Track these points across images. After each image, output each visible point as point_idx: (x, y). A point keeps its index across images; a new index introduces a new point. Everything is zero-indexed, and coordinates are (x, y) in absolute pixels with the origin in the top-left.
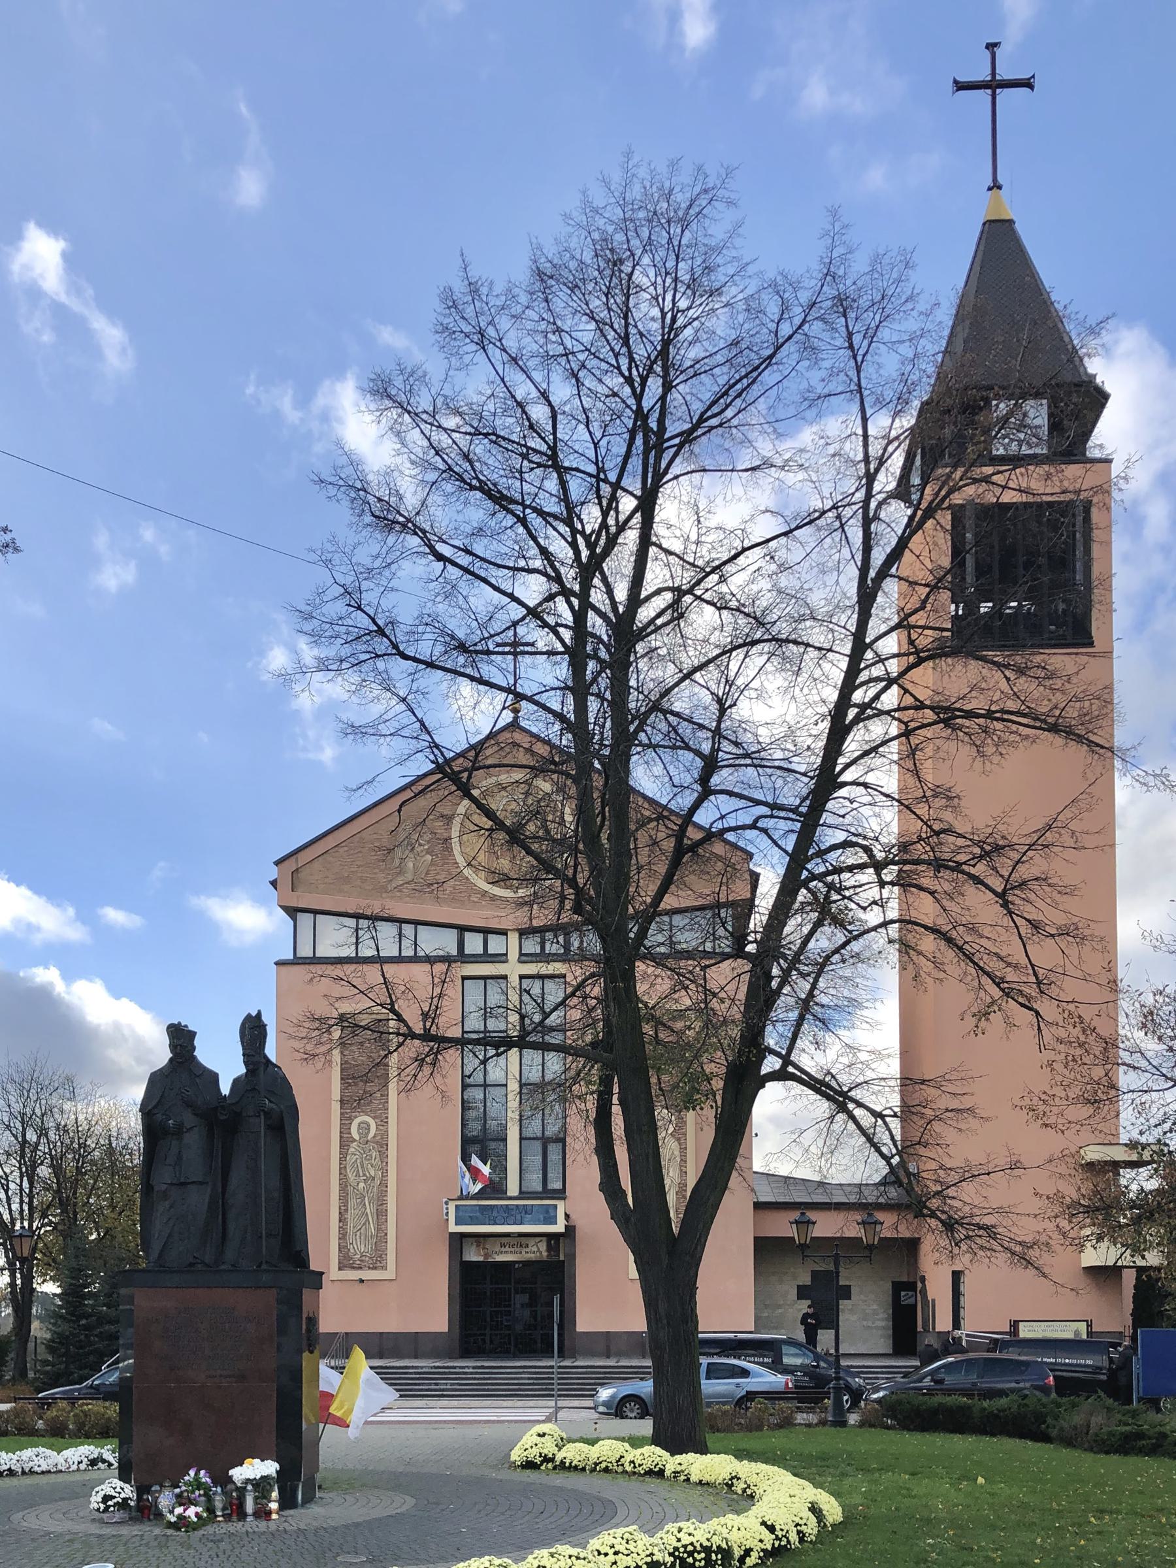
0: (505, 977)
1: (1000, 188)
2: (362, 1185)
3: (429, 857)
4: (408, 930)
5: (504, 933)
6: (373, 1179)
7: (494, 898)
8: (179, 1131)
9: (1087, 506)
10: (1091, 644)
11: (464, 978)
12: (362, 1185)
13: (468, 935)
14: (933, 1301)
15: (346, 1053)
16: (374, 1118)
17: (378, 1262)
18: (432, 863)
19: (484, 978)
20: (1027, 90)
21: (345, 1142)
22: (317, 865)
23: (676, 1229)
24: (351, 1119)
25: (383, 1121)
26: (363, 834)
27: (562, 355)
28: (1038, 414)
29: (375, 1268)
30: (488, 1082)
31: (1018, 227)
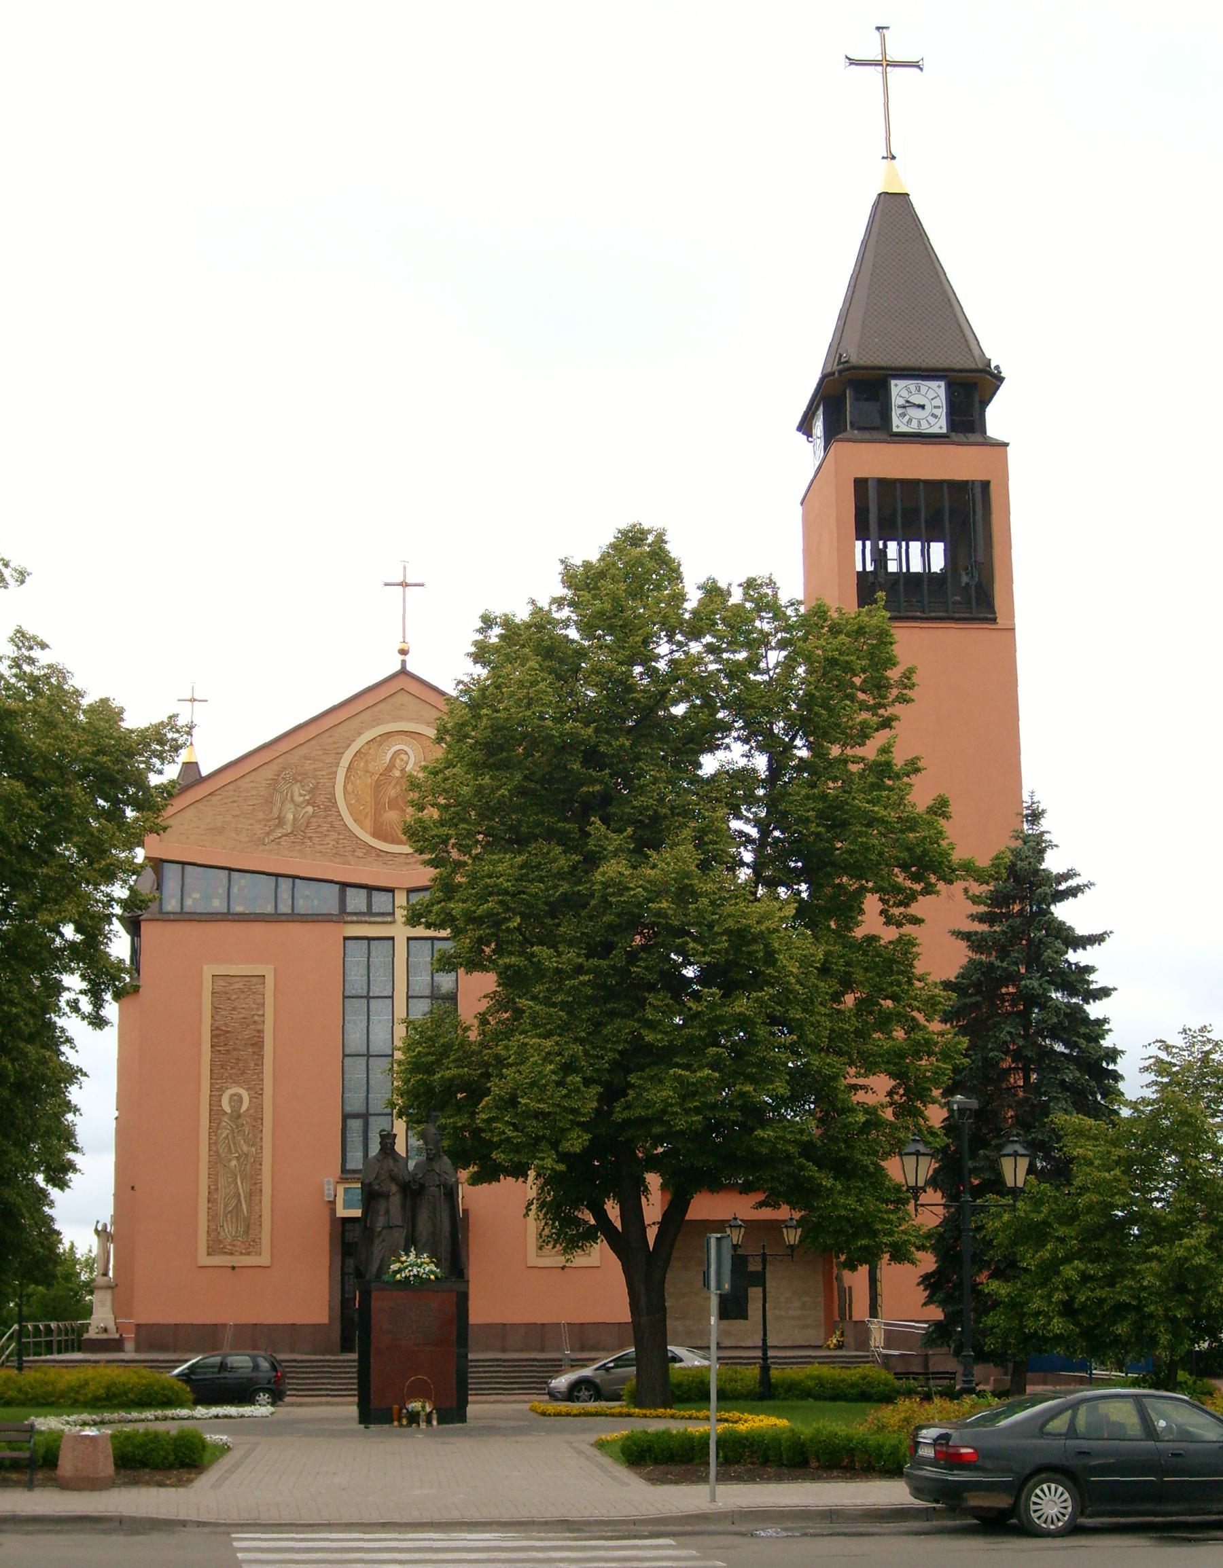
0: (392, 938)
1: (893, 158)
2: (234, 1163)
3: (310, 809)
4: (285, 885)
5: (391, 890)
6: (247, 1155)
7: (380, 853)
8: (386, 1196)
9: (986, 485)
10: (994, 620)
11: (346, 938)
12: (234, 1163)
13: (350, 891)
14: (850, 1288)
15: (218, 1018)
16: (248, 1089)
17: (252, 1246)
18: (314, 816)
19: (369, 939)
20: (916, 70)
21: (215, 1112)
22: (188, 814)
23: (620, 1229)
24: (222, 1090)
25: (257, 1094)
26: (240, 783)
27: (764, 1341)
28: (934, 394)
29: (249, 1254)
30: (372, 1053)
31: (914, 199)
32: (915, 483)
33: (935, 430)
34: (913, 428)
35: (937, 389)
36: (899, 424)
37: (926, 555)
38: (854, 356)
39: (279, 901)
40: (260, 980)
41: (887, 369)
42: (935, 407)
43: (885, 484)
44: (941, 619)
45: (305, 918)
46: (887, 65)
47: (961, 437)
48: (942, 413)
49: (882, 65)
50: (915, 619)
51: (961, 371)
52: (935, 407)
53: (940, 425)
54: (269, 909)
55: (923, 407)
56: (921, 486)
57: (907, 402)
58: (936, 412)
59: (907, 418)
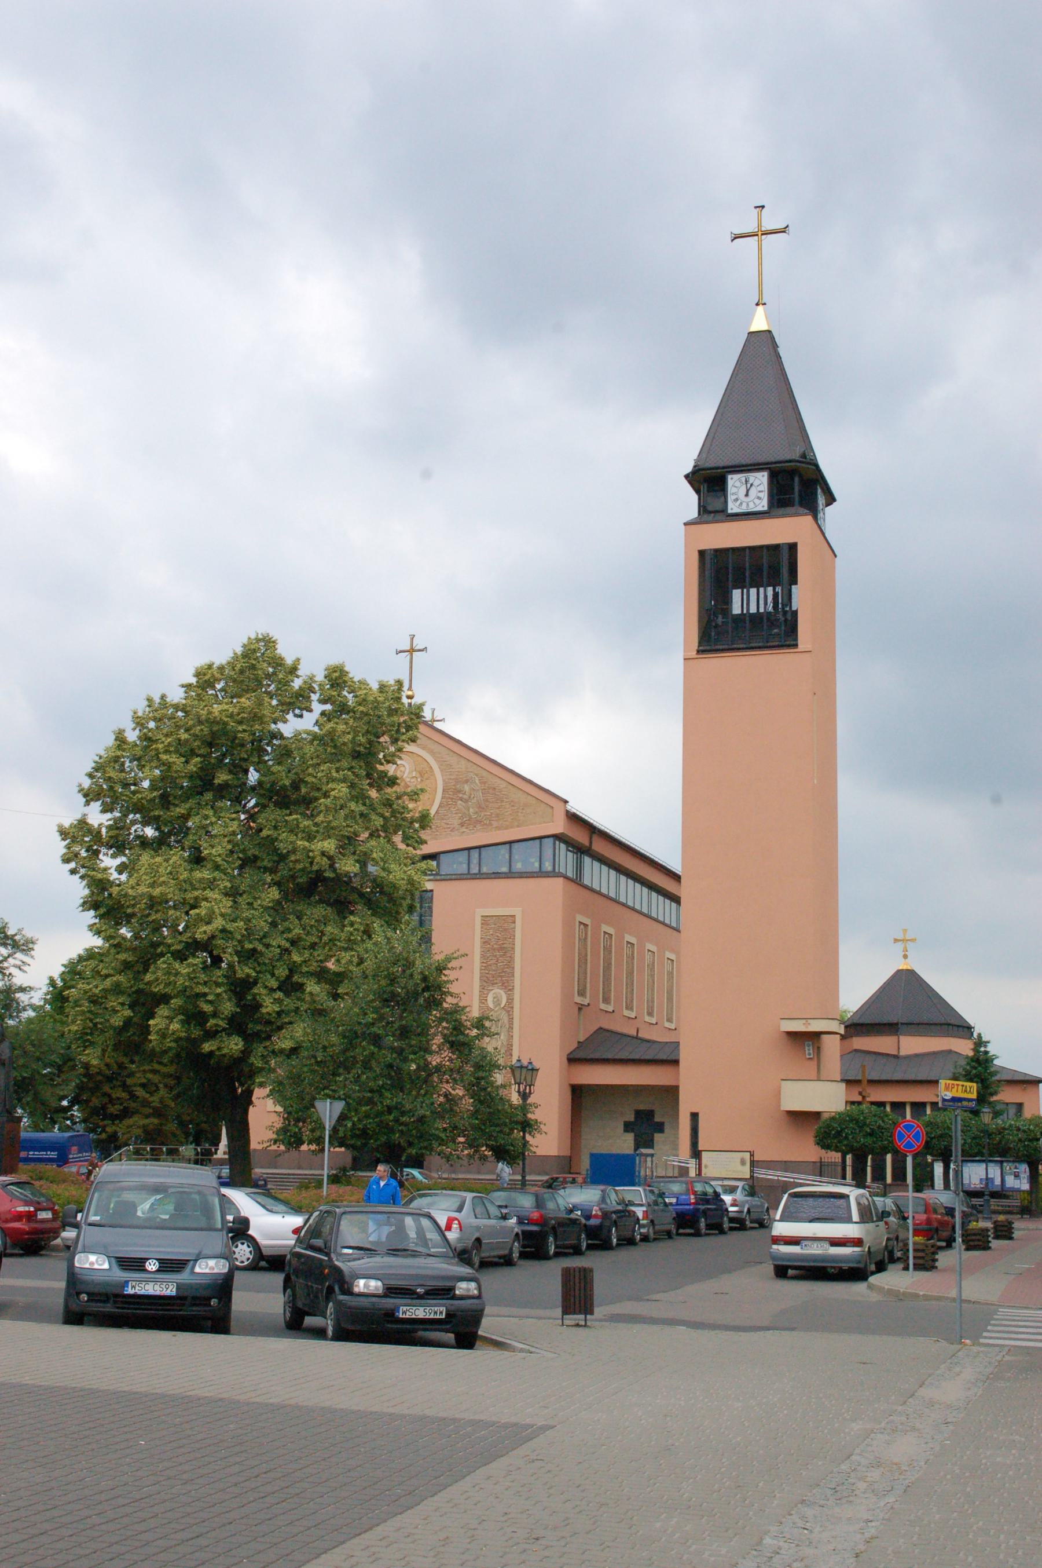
32: (742, 549)
33: (759, 508)
34: (744, 509)
35: (761, 478)
36: (733, 508)
37: (746, 601)
38: (702, 465)
39: (552, 860)
40: (510, 919)
41: (724, 468)
42: (760, 492)
43: (719, 552)
44: (760, 648)
45: (501, 875)
46: (762, 234)
47: (782, 511)
48: (765, 496)
49: (757, 235)
50: (738, 649)
51: (775, 463)
52: (760, 492)
53: (763, 505)
54: (505, 869)
55: (747, 495)
56: (747, 550)
57: (752, 485)
58: (761, 495)
59: (739, 502)
